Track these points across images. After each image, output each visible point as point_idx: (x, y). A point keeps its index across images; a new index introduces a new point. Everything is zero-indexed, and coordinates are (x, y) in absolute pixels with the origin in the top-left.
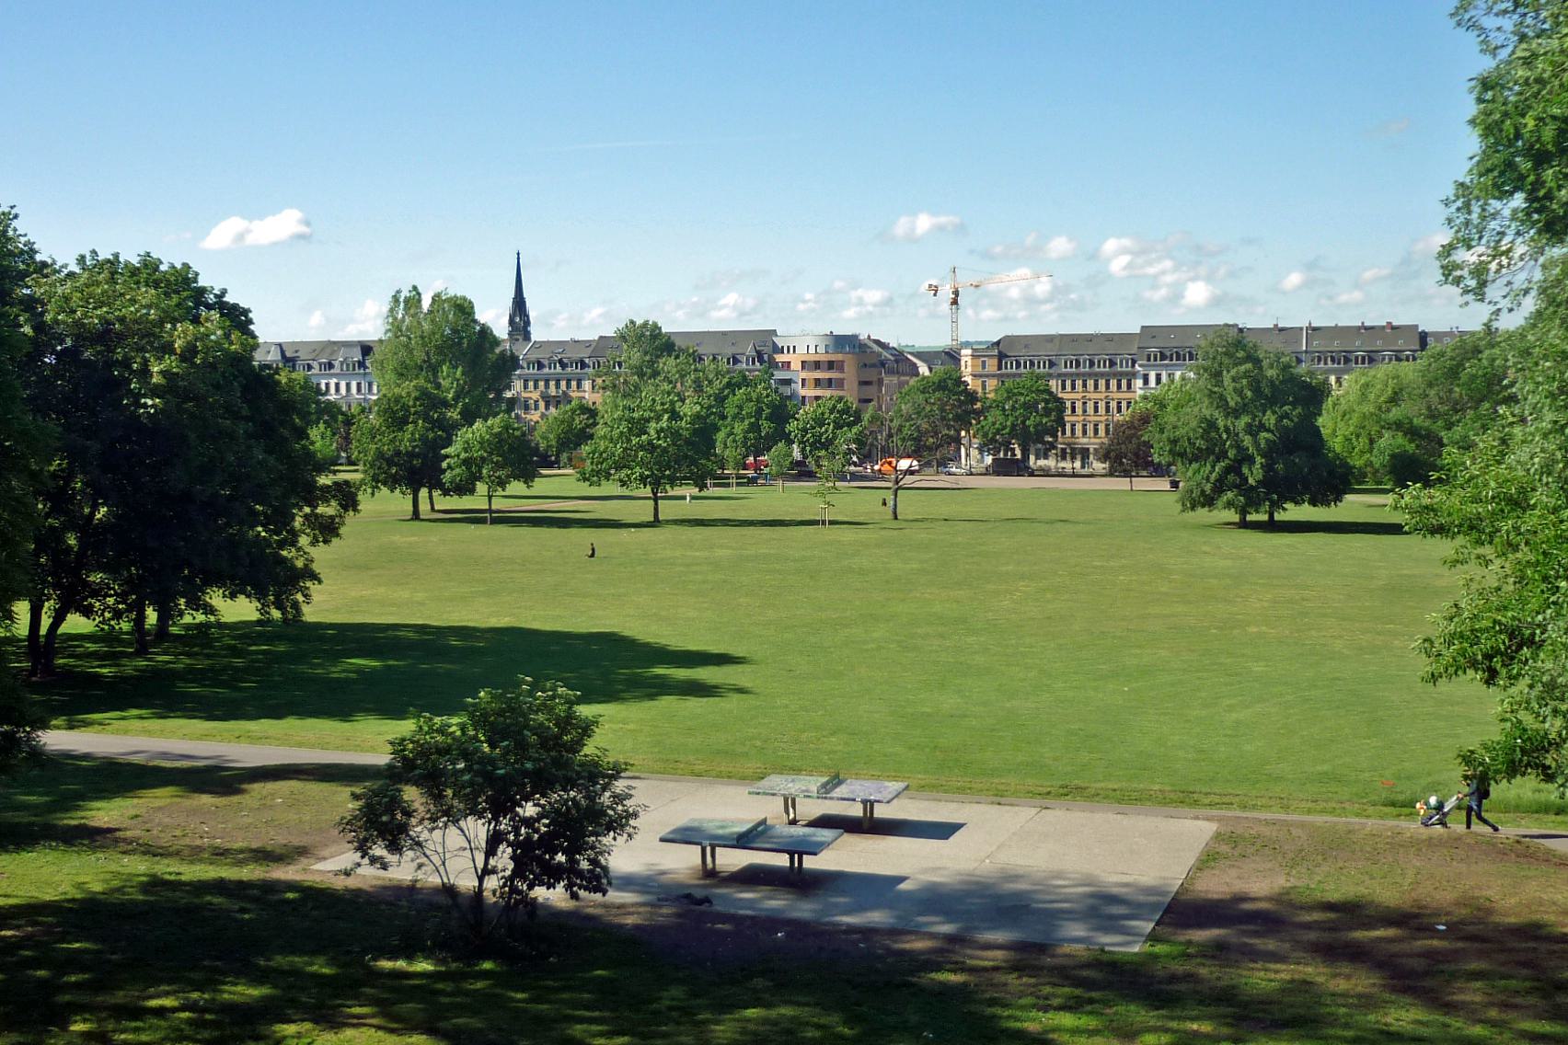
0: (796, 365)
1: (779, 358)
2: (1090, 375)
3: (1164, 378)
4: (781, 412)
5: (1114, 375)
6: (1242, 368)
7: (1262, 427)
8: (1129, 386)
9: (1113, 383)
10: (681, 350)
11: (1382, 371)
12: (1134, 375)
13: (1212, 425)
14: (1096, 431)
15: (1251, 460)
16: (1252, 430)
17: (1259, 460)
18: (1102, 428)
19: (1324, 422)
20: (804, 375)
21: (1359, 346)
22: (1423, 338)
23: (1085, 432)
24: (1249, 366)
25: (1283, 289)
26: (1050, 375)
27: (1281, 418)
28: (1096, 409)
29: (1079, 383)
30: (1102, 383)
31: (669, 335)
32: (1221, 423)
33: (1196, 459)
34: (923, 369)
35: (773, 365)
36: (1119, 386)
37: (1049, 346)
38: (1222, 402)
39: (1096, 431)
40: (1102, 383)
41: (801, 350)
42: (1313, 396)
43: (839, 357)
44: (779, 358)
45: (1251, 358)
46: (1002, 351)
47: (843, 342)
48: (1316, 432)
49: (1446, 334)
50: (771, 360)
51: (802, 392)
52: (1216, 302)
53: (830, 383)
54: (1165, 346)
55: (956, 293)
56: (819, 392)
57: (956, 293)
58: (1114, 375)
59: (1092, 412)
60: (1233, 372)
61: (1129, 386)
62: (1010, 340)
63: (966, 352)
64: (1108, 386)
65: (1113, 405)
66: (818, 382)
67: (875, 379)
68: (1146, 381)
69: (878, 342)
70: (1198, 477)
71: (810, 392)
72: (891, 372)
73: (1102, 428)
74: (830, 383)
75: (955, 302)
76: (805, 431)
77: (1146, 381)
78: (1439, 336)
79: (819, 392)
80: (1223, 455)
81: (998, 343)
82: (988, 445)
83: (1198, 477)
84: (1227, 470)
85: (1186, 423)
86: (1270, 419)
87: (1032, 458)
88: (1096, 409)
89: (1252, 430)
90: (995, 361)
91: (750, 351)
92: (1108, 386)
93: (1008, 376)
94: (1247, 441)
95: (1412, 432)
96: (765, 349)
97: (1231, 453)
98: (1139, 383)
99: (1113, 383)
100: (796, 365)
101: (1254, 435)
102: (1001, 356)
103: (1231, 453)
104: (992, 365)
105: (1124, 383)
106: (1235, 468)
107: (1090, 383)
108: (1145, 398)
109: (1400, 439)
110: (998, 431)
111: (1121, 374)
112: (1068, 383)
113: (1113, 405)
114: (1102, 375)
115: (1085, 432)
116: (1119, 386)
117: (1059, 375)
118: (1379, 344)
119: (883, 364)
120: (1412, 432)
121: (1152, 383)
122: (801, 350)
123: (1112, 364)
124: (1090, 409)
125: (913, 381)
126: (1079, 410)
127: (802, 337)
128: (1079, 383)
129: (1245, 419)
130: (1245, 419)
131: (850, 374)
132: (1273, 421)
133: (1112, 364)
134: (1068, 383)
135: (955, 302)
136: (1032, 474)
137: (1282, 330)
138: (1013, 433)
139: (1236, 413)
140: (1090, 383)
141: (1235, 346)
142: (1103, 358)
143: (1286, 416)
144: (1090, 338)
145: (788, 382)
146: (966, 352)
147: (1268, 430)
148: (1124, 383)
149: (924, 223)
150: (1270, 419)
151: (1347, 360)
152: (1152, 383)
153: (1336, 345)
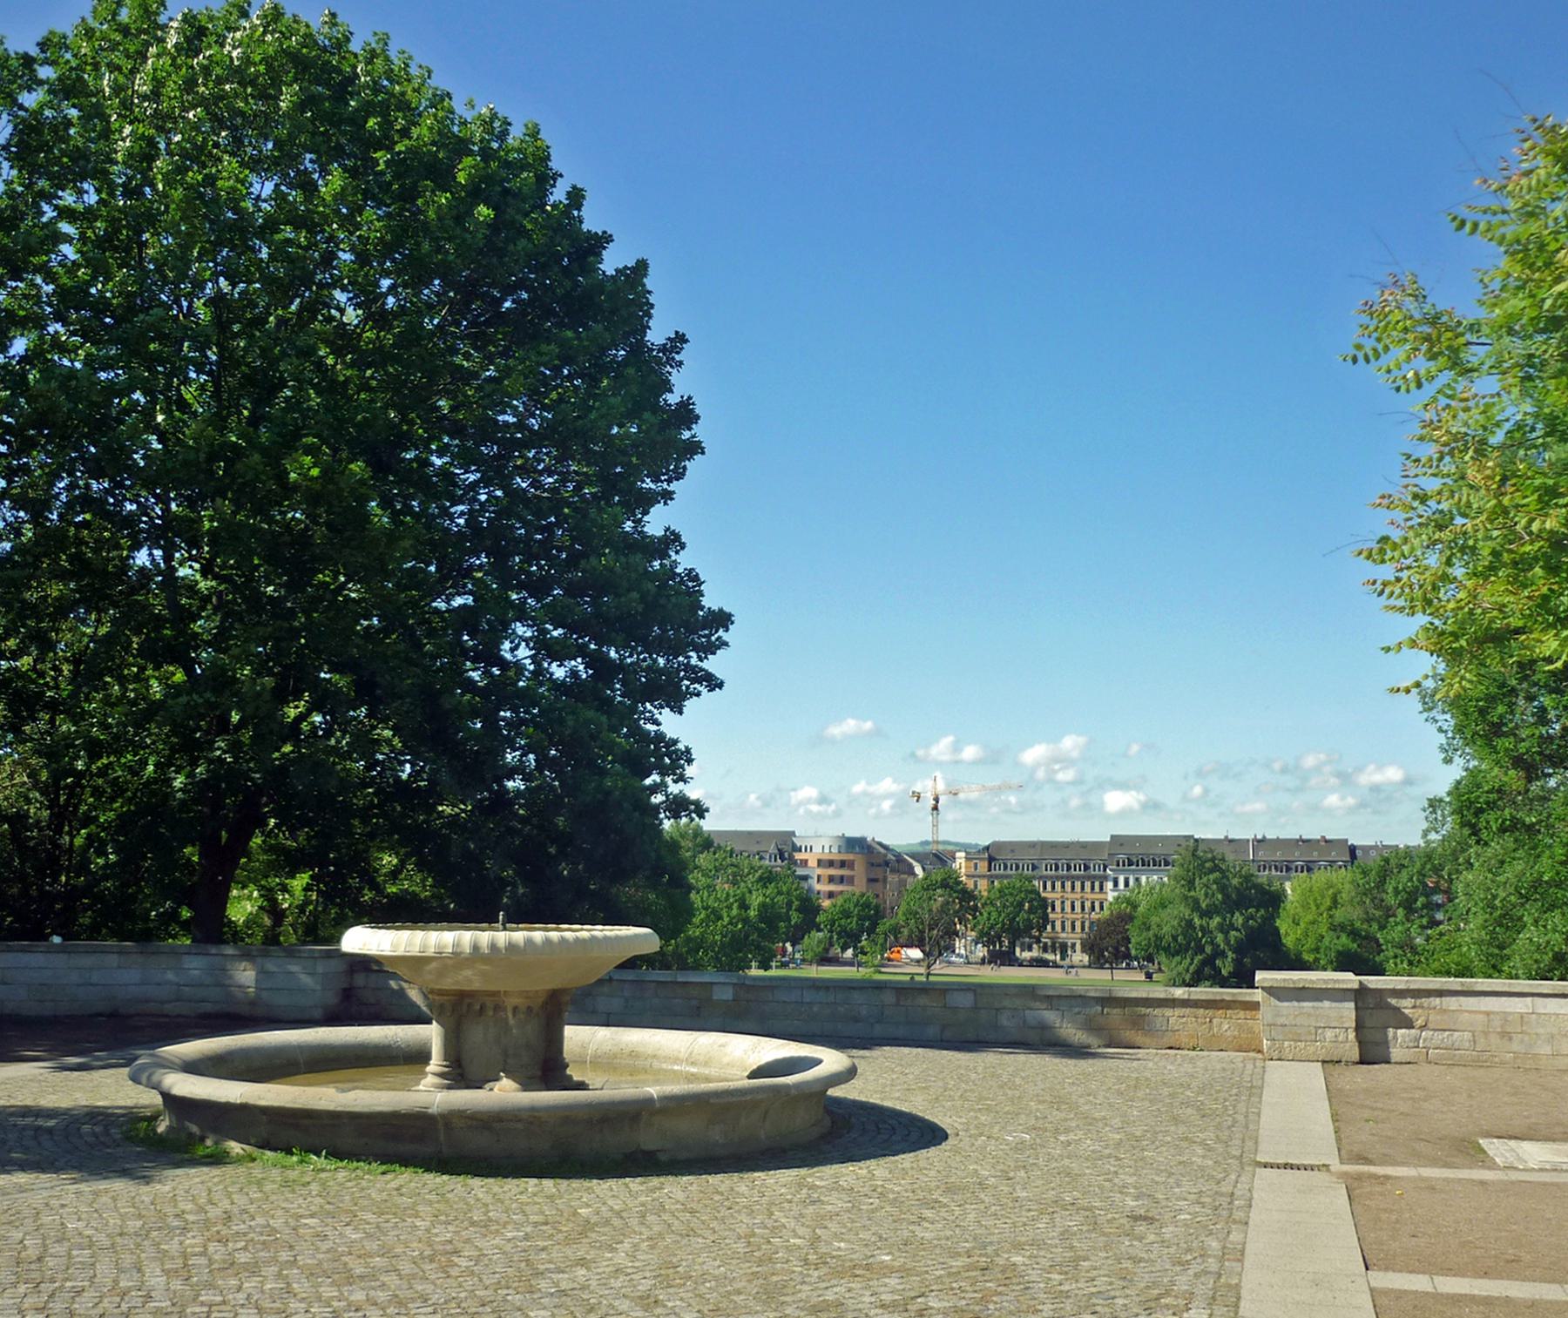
0: (812, 863)
1: (798, 856)
2: (1068, 878)
3: (1131, 883)
4: (809, 907)
5: (1058, 878)
6: (1211, 877)
7: (1233, 927)
8: (1101, 888)
9: (1088, 884)
10: (719, 847)
11: (1320, 877)
12: (1106, 878)
13: (1190, 924)
14: (1073, 928)
15: (1223, 954)
16: (1225, 929)
17: (1230, 955)
18: (1078, 925)
19: (1283, 925)
20: (819, 871)
21: (1298, 857)
22: (1353, 850)
23: (1063, 929)
24: (1217, 874)
25: (1237, 808)
26: (1034, 877)
27: (1247, 919)
28: (1073, 908)
29: (1058, 884)
30: (1078, 884)
31: (710, 833)
32: (1197, 922)
33: (1177, 953)
34: (918, 870)
35: (792, 861)
36: (1093, 888)
37: (1032, 851)
38: (1196, 905)
39: (1073, 928)
40: (1078, 884)
41: (817, 849)
42: (1274, 900)
43: (851, 857)
44: (798, 856)
45: (1216, 868)
46: (991, 855)
47: (855, 844)
48: (1277, 930)
49: (1371, 847)
50: (791, 857)
51: (818, 887)
52: (1151, 806)
53: (842, 880)
54: (1134, 854)
55: (937, 799)
56: (832, 888)
57: (937, 799)
58: (1089, 878)
59: (1073, 909)
60: (1205, 880)
61: (1101, 888)
62: (998, 846)
63: (961, 855)
64: (1083, 888)
65: (1088, 905)
66: (831, 879)
67: (880, 877)
68: (1116, 884)
69: (880, 844)
70: (1180, 968)
71: (824, 888)
72: (893, 871)
73: (1078, 925)
74: (842, 880)
75: (935, 808)
76: (833, 922)
77: (1116, 884)
78: (1366, 849)
79: (832, 888)
80: (1200, 949)
81: (987, 848)
82: (986, 938)
83: (1180, 968)
84: (1204, 963)
85: (1168, 923)
86: (1238, 919)
87: (1018, 950)
88: (1073, 908)
89: (1225, 929)
90: (986, 864)
91: (772, 849)
92: (1083, 888)
93: (997, 877)
94: (1220, 938)
95: (1354, 934)
96: (786, 847)
97: (1208, 949)
98: (1110, 885)
99: (1088, 884)
100: (812, 863)
101: (1226, 931)
102: (991, 860)
103: (1208, 949)
104: (983, 867)
105: (1097, 884)
106: (1209, 961)
107: (1068, 884)
108: (1117, 899)
109: (1344, 939)
110: (992, 927)
111: (1095, 877)
112: (1049, 884)
113: (1088, 905)
114: (1078, 878)
115: (1063, 929)
116: (1093, 888)
117: (1040, 878)
118: (1315, 856)
119: (887, 864)
120: (1354, 934)
121: (1121, 885)
122: (817, 849)
123: (1087, 868)
124: (1068, 908)
125: (910, 879)
126: (1058, 909)
127: (818, 838)
128: (1058, 884)
129: (1217, 920)
130: (1217, 920)
131: (859, 872)
132: (1241, 921)
133: (1087, 868)
134: (1049, 884)
135: (935, 808)
136: (1021, 965)
137: (1231, 841)
138: (1003, 930)
139: (1207, 914)
140: (1068, 884)
141: (1200, 859)
142: (1081, 862)
143: (1252, 917)
144: (1066, 846)
145: (805, 878)
146: (961, 855)
147: (1237, 930)
148: (1097, 884)
149: (850, 725)
150: (1238, 919)
151: (1288, 869)
152: (1121, 885)
153: (1279, 856)
